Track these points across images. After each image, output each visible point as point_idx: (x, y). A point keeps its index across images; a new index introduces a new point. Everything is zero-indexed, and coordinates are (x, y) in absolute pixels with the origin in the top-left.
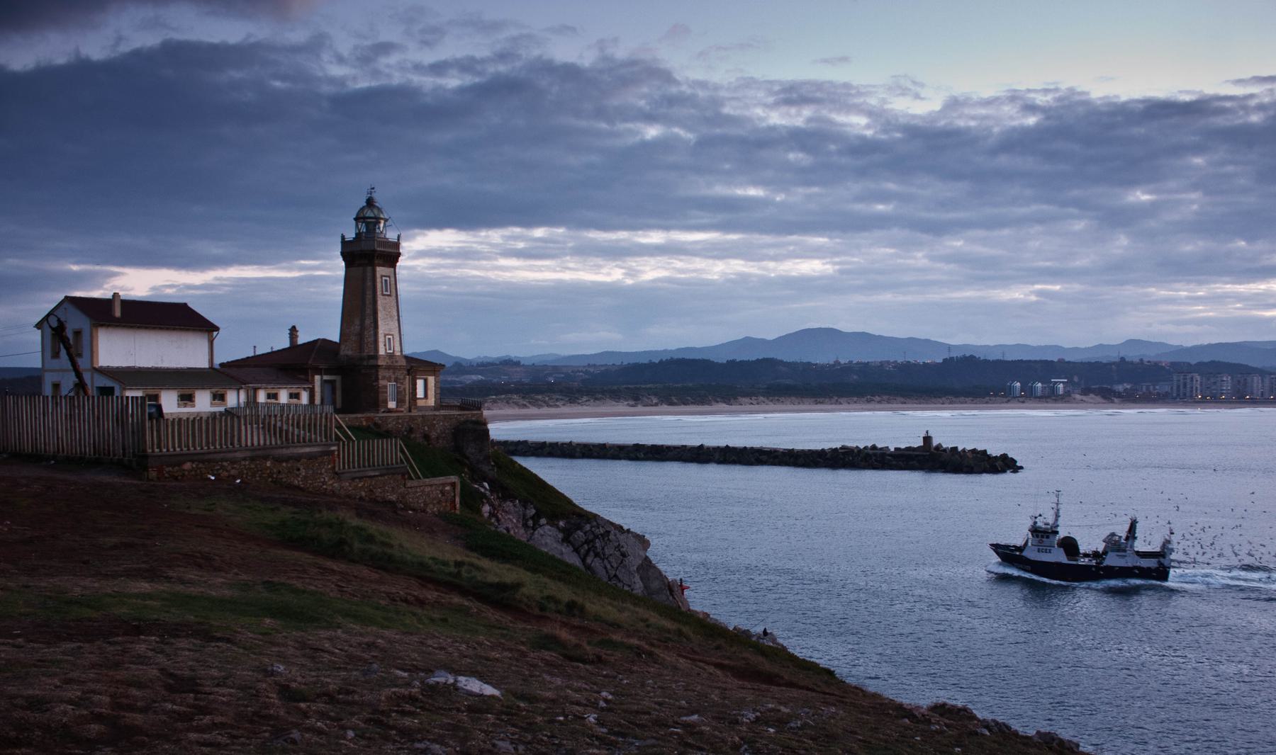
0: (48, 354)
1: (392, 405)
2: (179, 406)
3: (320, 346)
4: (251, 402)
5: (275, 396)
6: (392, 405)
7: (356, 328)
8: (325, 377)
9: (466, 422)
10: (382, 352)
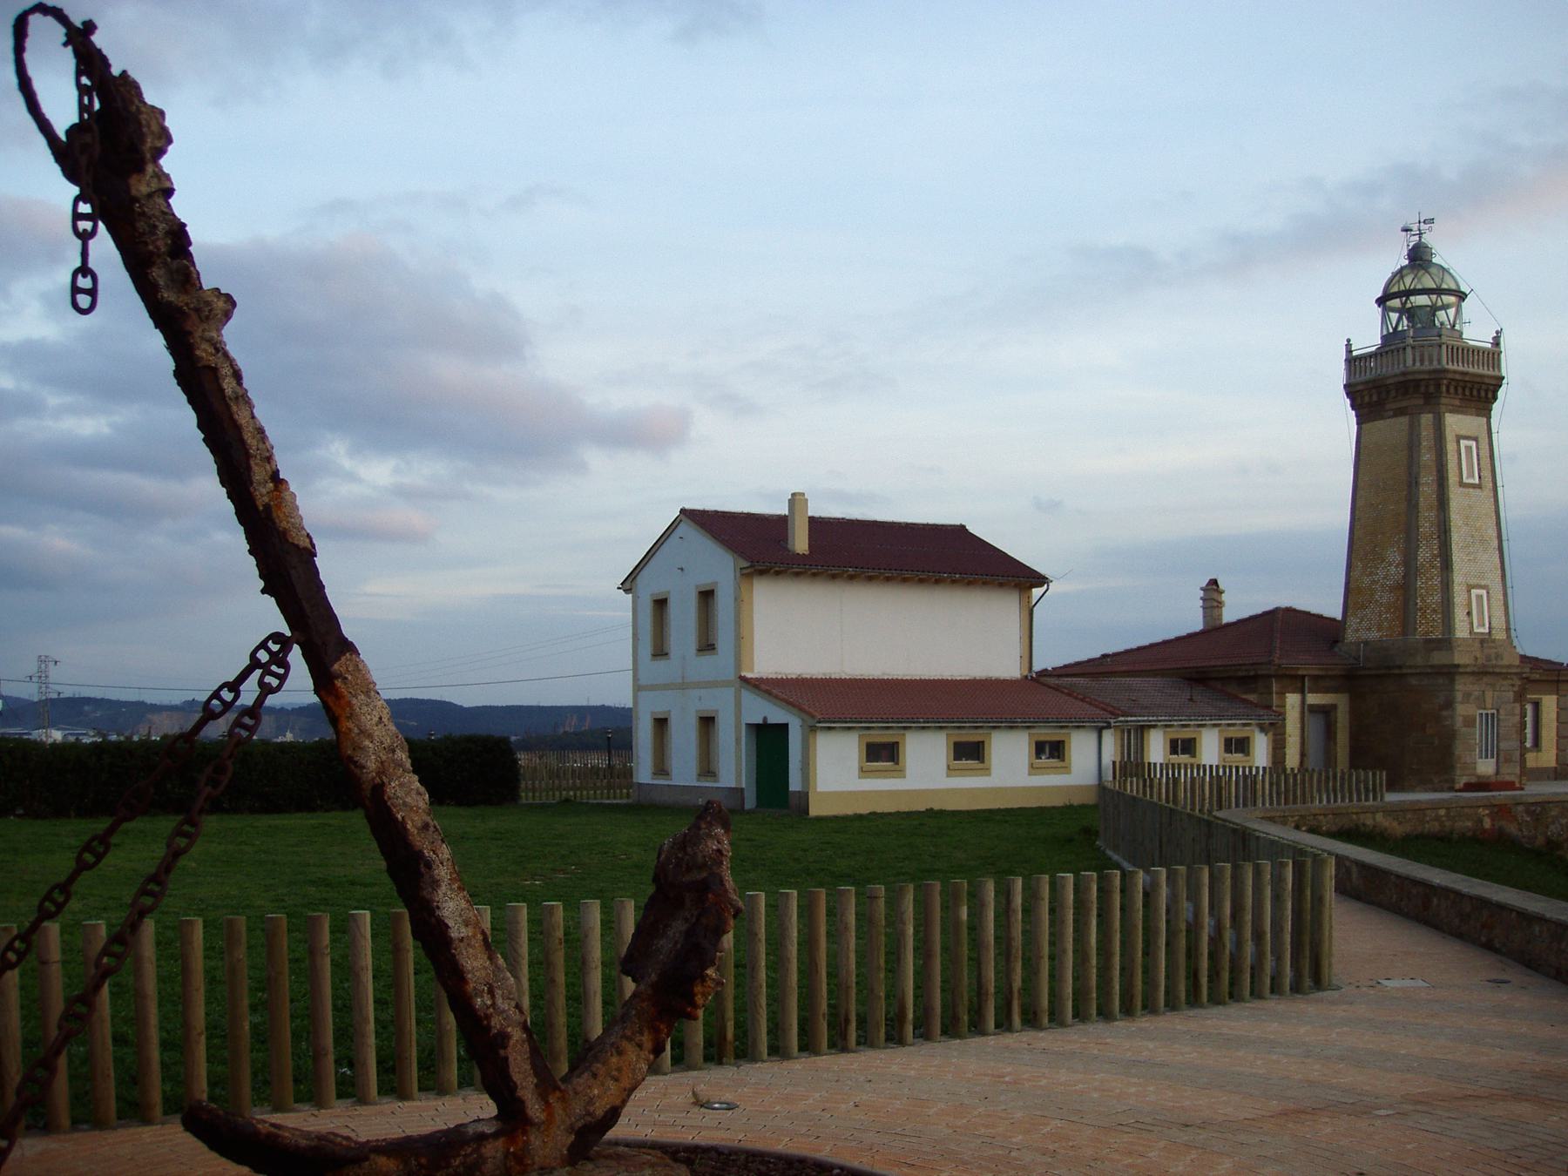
0: (647, 649)
2: (863, 772)
3: (1284, 626)
4: (1132, 765)
8: (1313, 699)
10: (1461, 632)
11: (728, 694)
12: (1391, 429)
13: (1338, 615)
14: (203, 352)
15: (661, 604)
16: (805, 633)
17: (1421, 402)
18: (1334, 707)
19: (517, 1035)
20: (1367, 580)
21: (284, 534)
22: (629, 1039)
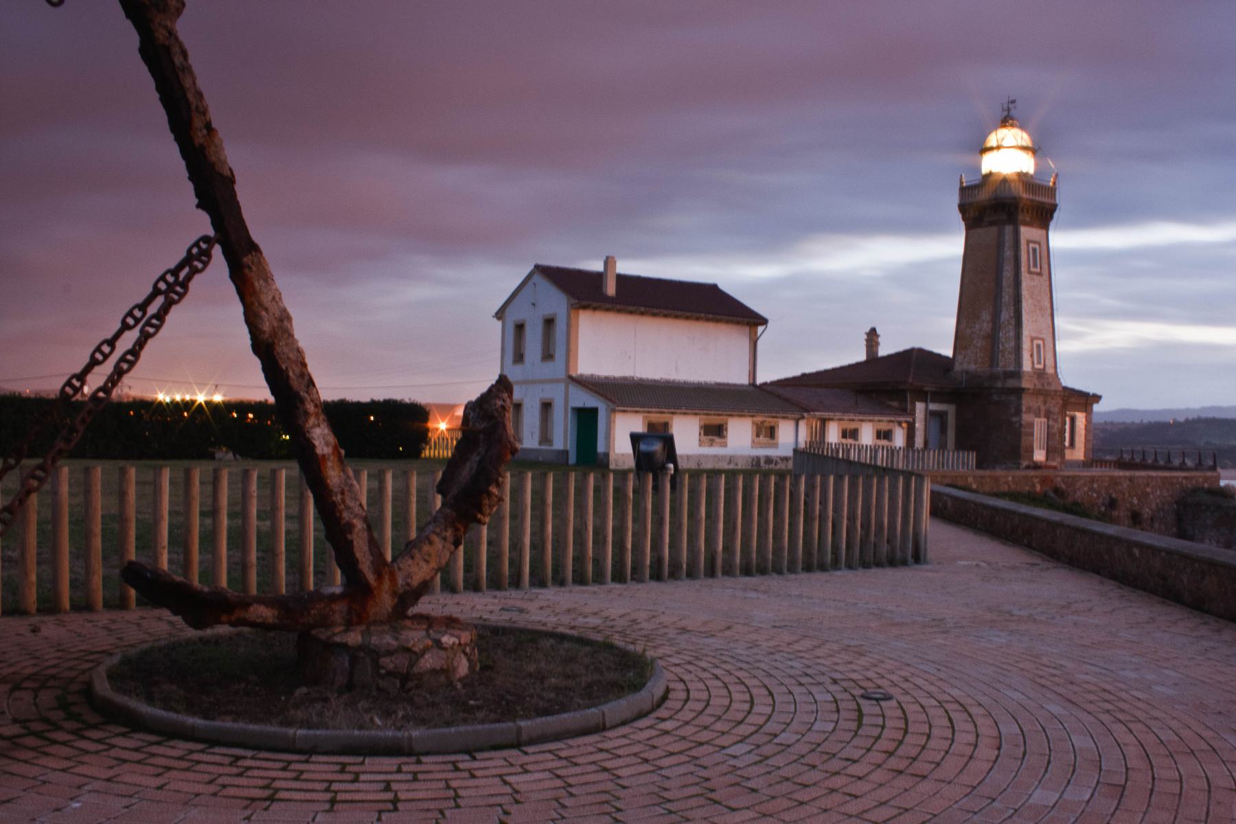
1: (1039, 456)
2: (701, 444)
3: (915, 359)
5: (854, 434)
6: (1039, 456)
7: (984, 324)
8: (933, 407)
9: (1195, 491)
10: (1027, 366)
11: (562, 386)
12: (988, 234)
13: (948, 352)
14: (161, 35)
15: (520, 328)
16: (608, 348)
17: (1005, 217)
18: (946, 413)
19: (359, 525)
20: (968, 331)
21: (213, 166)
22: (438, 535)
